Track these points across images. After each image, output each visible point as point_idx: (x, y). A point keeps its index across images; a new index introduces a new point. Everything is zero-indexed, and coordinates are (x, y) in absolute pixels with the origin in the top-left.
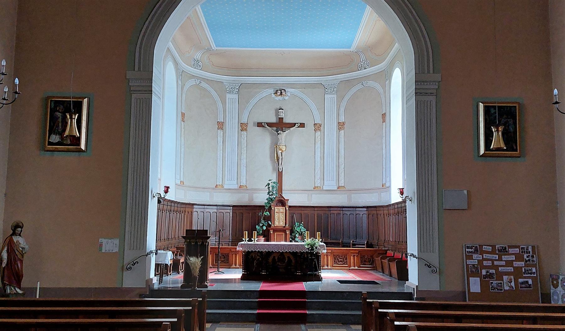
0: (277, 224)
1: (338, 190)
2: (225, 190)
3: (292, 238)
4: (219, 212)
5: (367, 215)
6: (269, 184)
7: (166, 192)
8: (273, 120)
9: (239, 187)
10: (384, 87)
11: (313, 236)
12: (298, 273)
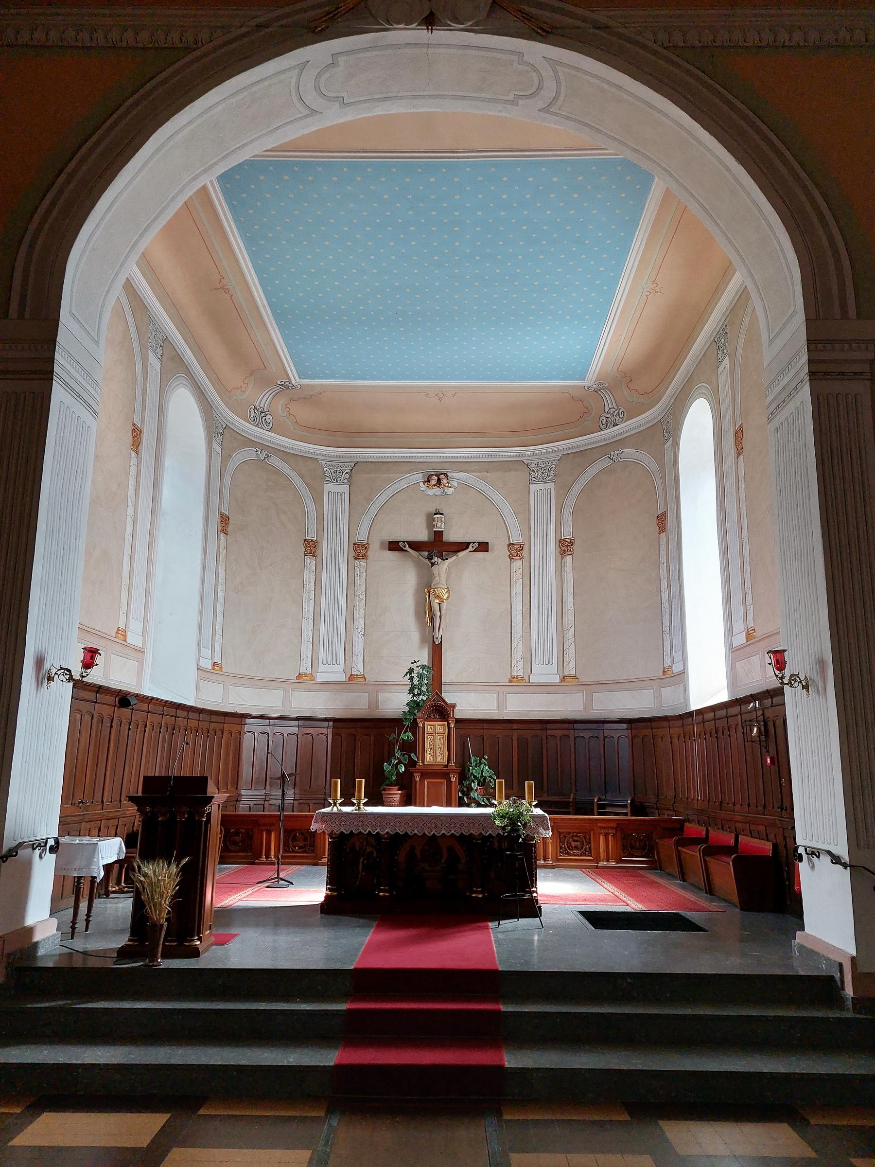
0: (429, 759)
1: (561, 684)
2: (316, 686)
3: (463, 792)
4: (303, 735)
5: (629, 740)
6: (411, 671)
7: (88, 665)
8: (422, 535)
9: (349, 678)
10: (660, 458)
11: (515, 792)
12: (476, 892)
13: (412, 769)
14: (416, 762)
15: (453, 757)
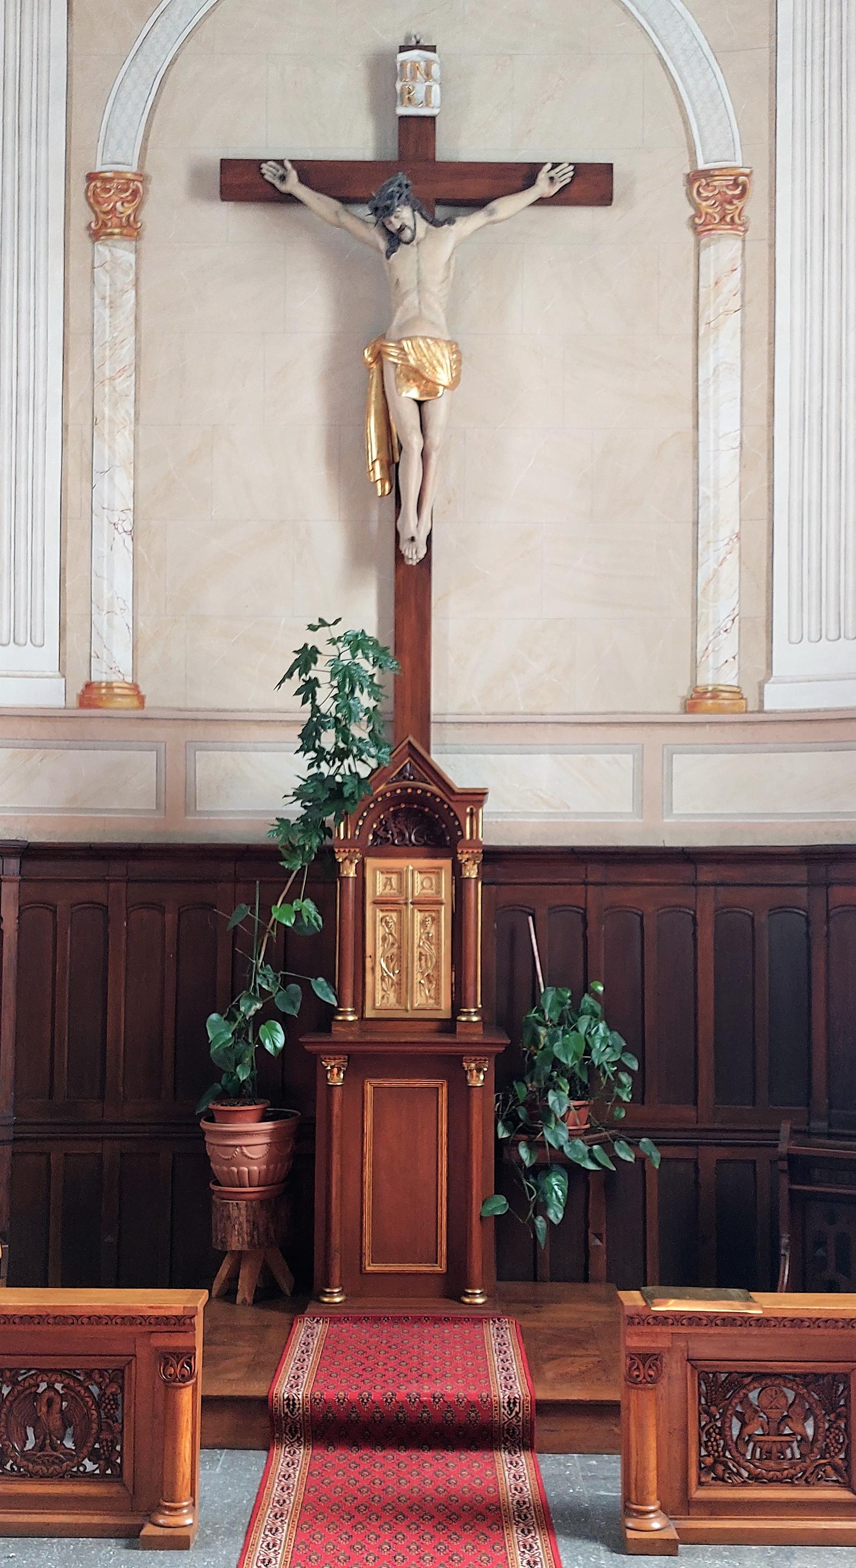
3: (511, 1121)
13: (311, 1042)
14: (330, 1012)
15: (476, 989)
